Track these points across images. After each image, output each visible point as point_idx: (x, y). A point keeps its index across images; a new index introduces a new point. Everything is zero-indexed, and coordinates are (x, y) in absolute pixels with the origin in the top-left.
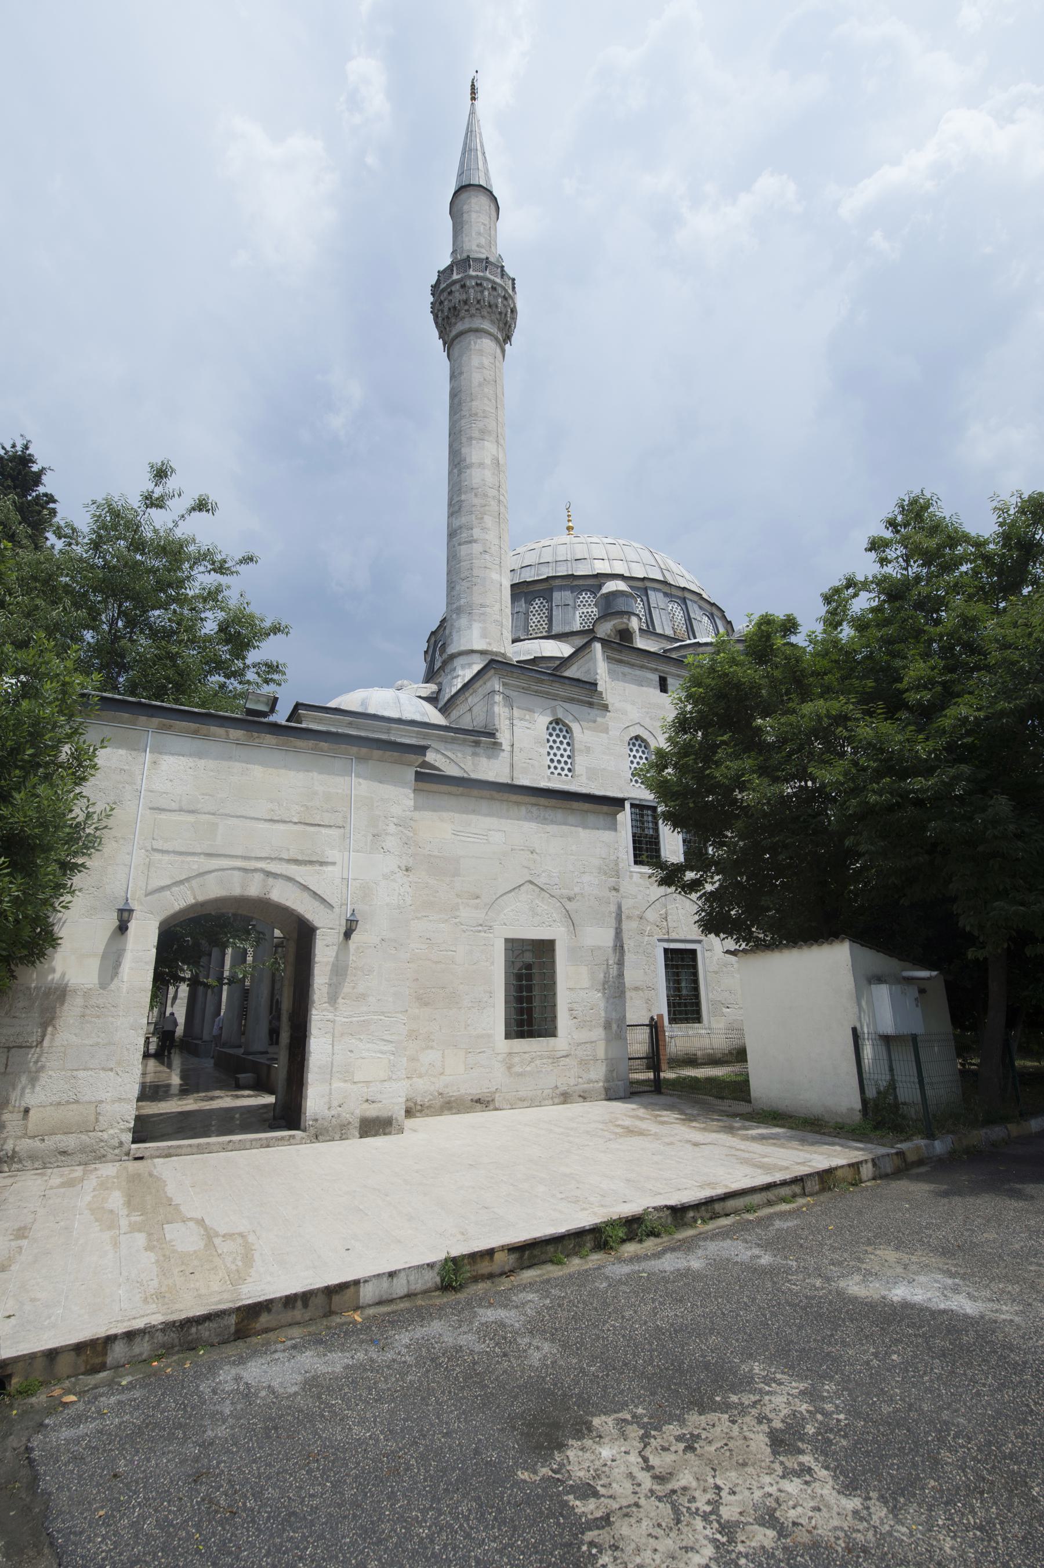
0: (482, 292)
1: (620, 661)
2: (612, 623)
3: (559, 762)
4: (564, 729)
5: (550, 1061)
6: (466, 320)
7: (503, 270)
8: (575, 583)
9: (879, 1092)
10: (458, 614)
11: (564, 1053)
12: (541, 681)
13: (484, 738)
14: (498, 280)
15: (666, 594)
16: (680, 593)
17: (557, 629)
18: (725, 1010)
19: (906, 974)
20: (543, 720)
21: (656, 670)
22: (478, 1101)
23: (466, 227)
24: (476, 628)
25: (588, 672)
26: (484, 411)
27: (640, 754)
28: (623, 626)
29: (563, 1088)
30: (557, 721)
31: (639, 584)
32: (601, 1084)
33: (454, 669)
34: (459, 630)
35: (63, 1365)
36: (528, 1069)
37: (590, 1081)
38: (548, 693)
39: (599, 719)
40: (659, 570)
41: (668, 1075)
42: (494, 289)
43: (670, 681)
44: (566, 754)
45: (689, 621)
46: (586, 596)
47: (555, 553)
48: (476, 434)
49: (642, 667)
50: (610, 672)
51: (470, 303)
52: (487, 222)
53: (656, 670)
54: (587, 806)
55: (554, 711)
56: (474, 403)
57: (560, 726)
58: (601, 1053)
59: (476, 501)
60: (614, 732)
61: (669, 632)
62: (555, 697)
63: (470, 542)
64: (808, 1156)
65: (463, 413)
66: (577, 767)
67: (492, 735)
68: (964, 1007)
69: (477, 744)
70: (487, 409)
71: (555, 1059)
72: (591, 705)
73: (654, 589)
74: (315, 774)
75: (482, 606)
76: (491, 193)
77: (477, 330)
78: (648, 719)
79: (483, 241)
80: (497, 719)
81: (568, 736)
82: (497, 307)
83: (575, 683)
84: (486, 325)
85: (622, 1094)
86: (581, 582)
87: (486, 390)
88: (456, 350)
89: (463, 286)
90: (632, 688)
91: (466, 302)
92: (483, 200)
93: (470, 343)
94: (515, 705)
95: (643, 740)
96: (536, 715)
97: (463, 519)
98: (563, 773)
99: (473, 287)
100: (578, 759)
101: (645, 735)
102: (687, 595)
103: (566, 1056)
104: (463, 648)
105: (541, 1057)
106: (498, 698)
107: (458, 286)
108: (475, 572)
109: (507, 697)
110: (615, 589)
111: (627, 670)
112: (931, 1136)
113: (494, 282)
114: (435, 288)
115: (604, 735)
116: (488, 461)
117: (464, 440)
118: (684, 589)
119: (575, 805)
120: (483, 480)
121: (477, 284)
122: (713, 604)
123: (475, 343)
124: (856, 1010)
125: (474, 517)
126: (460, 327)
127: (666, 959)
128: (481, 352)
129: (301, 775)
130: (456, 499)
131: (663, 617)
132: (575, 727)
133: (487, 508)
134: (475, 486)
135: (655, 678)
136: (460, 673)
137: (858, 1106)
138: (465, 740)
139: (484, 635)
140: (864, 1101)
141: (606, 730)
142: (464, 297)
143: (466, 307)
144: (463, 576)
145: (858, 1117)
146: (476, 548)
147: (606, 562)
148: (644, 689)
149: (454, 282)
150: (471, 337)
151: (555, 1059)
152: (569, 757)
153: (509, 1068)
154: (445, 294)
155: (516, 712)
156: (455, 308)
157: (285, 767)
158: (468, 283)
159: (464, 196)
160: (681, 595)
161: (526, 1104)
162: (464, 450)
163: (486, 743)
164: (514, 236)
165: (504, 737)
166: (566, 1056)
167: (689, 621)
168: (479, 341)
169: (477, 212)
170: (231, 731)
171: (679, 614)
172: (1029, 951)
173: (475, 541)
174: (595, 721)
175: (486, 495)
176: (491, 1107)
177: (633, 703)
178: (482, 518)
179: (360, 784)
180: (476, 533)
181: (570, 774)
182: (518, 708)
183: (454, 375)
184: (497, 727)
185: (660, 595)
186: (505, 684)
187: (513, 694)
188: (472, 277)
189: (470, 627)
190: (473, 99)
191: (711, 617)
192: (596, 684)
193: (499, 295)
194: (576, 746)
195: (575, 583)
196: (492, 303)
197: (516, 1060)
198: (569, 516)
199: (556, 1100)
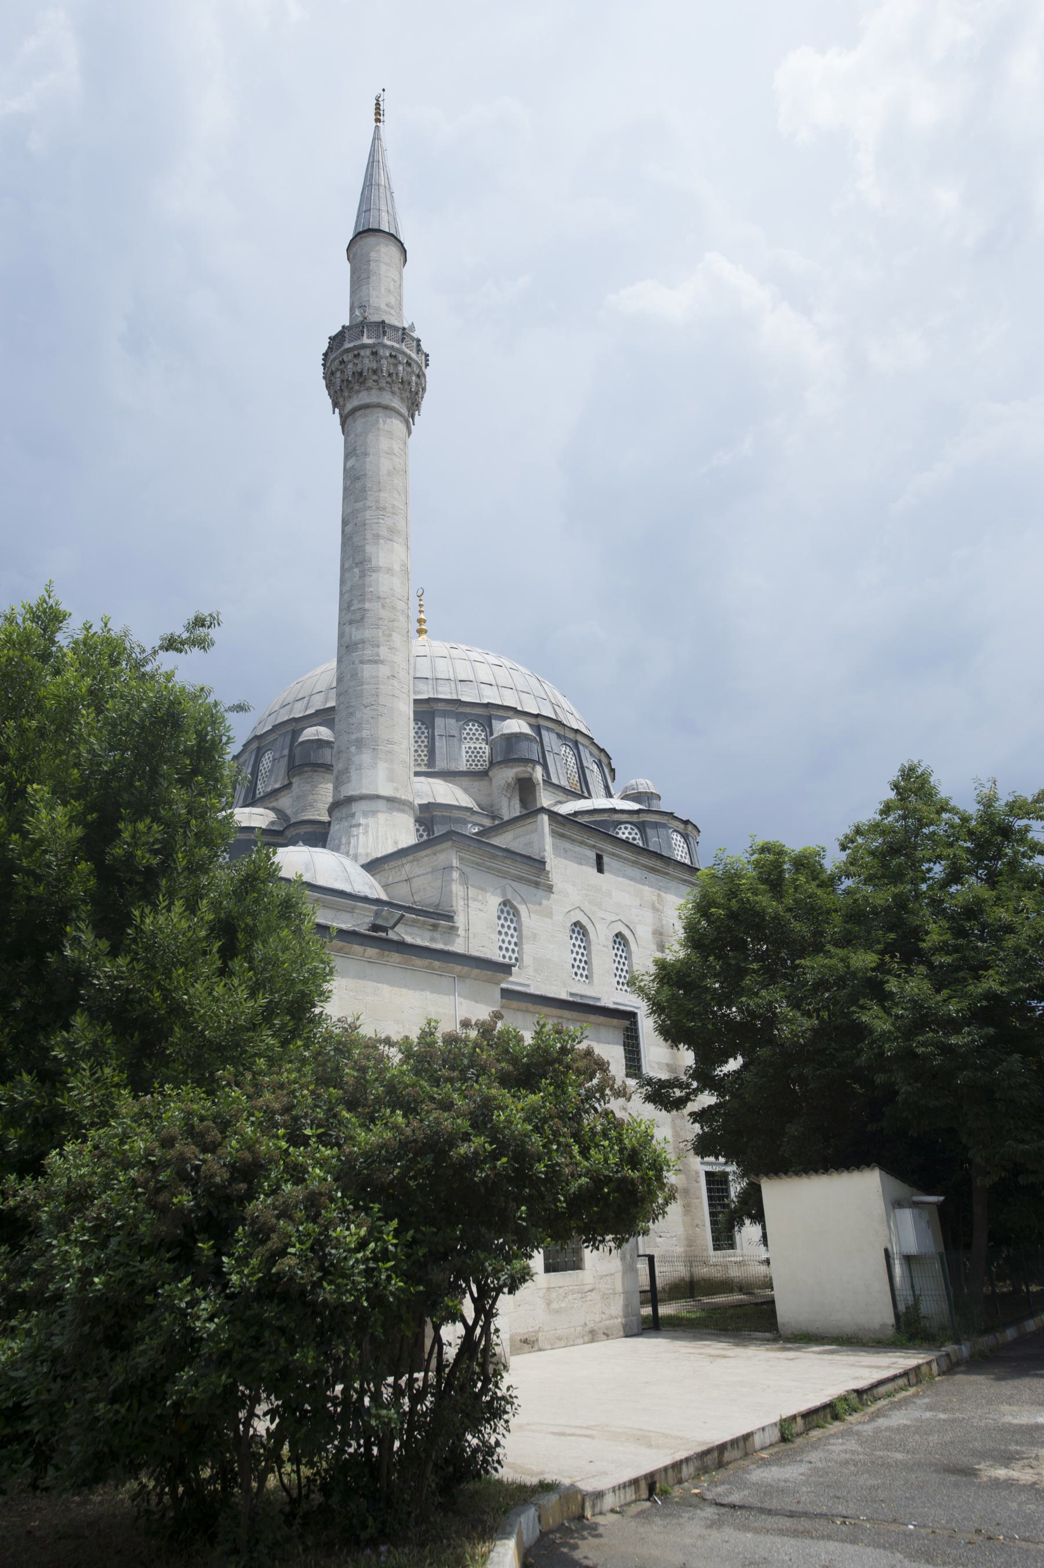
0: (396, 365)
1: (562, 836)
2: (515, 770)
3: (507, 949)
4: (511, 911)
5: (580, 1295)
6: (373, 392)
7: (419, 345)
8: (461, 710)
9: (907, 1308)
11: (590, 1287)
12: (494, 857)
13: (440, 917)
14: (414, 355)
15: (559, 735)
16: (571, 735)
17: (440, 765)
18: (659, 1240)
19: (916, 1198)
20: (494, 901)
21: (594, 846)
22: (525, 1341)
23: (373, 278)
24: (382, 768)
25: (530, 844)
26: (393, 506)
27: (579, 942)
28: (526, 775)
29: (590, 1325)
30: (505, 903)
31: (533, 721)
32: (619, 1320)
33: (353, 815)
34: (359, 768)
35: (687, 1471)
36: (563, 1305)
37: (611, 1317)
38: (499, 871)
39: (544, 902)
40: (550, 705)
41: (664, 1310)
42: (409, 364)
43: (606, 859)
45: (582, 769)
46: (473, 728)
47: (433, 668)
48: (384, 532)
49: (582, 843)
50: (555, 847)
51: (370, 371)
52: (396, 278)
53: (594, 846)
54: (602, 1019)
55: (504, 894)
56: (382, 494)
57: (508, 908)
58: (619, 1288)
59: (383, 613)
61: (564, 783)
63: (376, 662)
64: (894, 1360)
65: (368, 503)
67: (450, 918)
68: (953, 1227)
69: (435, 927)
70: (396, 503)
71: (584, 1293)
72: (537, 885)
73: (548, 729)
74: (428, 993)
75: (390, 742)
76: (402, 245)
77: (386, 408)
79: (393, 300)
80: (454, 899)
81: (515, 919)
82: (409, 383)
83: (525, 861)
84: (387, 399)
85: (636, 1331)
86: (468, 710)
87: (396, 481)
88: (359, 423)
89: (375, 353)
90: (573, 867)
91: (375, 372)
92: (393, 251)
93: (377, 421)
94: (470, 882)
95: (582, 927)
96: (488, 894)
97: (367, 631)
99: (386, 358)
100: (527, 947)
101: (585, 921)
102: (580, 739)
103: (591, 1291)
104: (365, 791)
105: (573, 1292)
106: (455, 875)
107: (368, 352)
108: (382, 700)
109: (463, 873)
110: (516, 730)
111: (567, 845)
112: (958, 1342)
113: (410, 358)
114: (336, 340)
116: (397, 568)
117: (369, 536)
118: (577, 731)
119: (593, 1018)
120: (392, 589)
121: (391, 355)
122: (602, 750)
123: (385, 423)
124: (887, 1232)
125: (380, 631)
126: (363, 398)
127: (708, 1183)
128: (390, 434)
129: (417, 994)
130: (356, 606)
131: (558, 764)
132: (522, 909)
133: (396, 624)
134: (382, 595)
135: (592, 855)
136: (362, 821)
137: (891, 1320)
138: (424, 923)
139: (391, 779)
140: (897, 1316)
141: (550, 915)
142: (374, 366)
143: (375, 377)
144: (365, 702)
145: (891, 1331)
146: (383, 670)
147: (448, 659)
148: (584, 867)
149: (365, 346)
150: (380, 414)
151: (584, 1293)
152: (516, 944)
153: (548, 1304)
154: (350, 356)
155: (472, 892)
156: (361, 374)
157: (406, 986)
158: (381, 352)
159: (371, 240)
160: (574, 739)
161: (563, 1343)
162: (369, 549)
163: (444, 927)
164: (419, 300)
165: (460, 920)
166: (591, 1291)
167: (582, 769)
168: (388, 420)
169: (386, 264)
170: (369, 949)
171: (572, 761)
172: (1022, 1180)
173: (382, 662)
174: (540, 904)
175: (394, 608)
176: (536, 1348)
178: (390, 636)
179: (461, 1004)
180: (383, 652)
182: (473, 886)
183: (350, 452)
184: (455, 908)
185: (553, 736)
186: (461, 859)
187: (467, 870)
188: (385, 346)
189: (374, 766)
190: (378, 120)
191: (600, 764)
192: (544, 863)
193: (413, 372)
194: (524, 932)
195: (461, 710)
196: (405, 379)
197: (554, 1295)
198: (420, 605)
199: (586, 1339)
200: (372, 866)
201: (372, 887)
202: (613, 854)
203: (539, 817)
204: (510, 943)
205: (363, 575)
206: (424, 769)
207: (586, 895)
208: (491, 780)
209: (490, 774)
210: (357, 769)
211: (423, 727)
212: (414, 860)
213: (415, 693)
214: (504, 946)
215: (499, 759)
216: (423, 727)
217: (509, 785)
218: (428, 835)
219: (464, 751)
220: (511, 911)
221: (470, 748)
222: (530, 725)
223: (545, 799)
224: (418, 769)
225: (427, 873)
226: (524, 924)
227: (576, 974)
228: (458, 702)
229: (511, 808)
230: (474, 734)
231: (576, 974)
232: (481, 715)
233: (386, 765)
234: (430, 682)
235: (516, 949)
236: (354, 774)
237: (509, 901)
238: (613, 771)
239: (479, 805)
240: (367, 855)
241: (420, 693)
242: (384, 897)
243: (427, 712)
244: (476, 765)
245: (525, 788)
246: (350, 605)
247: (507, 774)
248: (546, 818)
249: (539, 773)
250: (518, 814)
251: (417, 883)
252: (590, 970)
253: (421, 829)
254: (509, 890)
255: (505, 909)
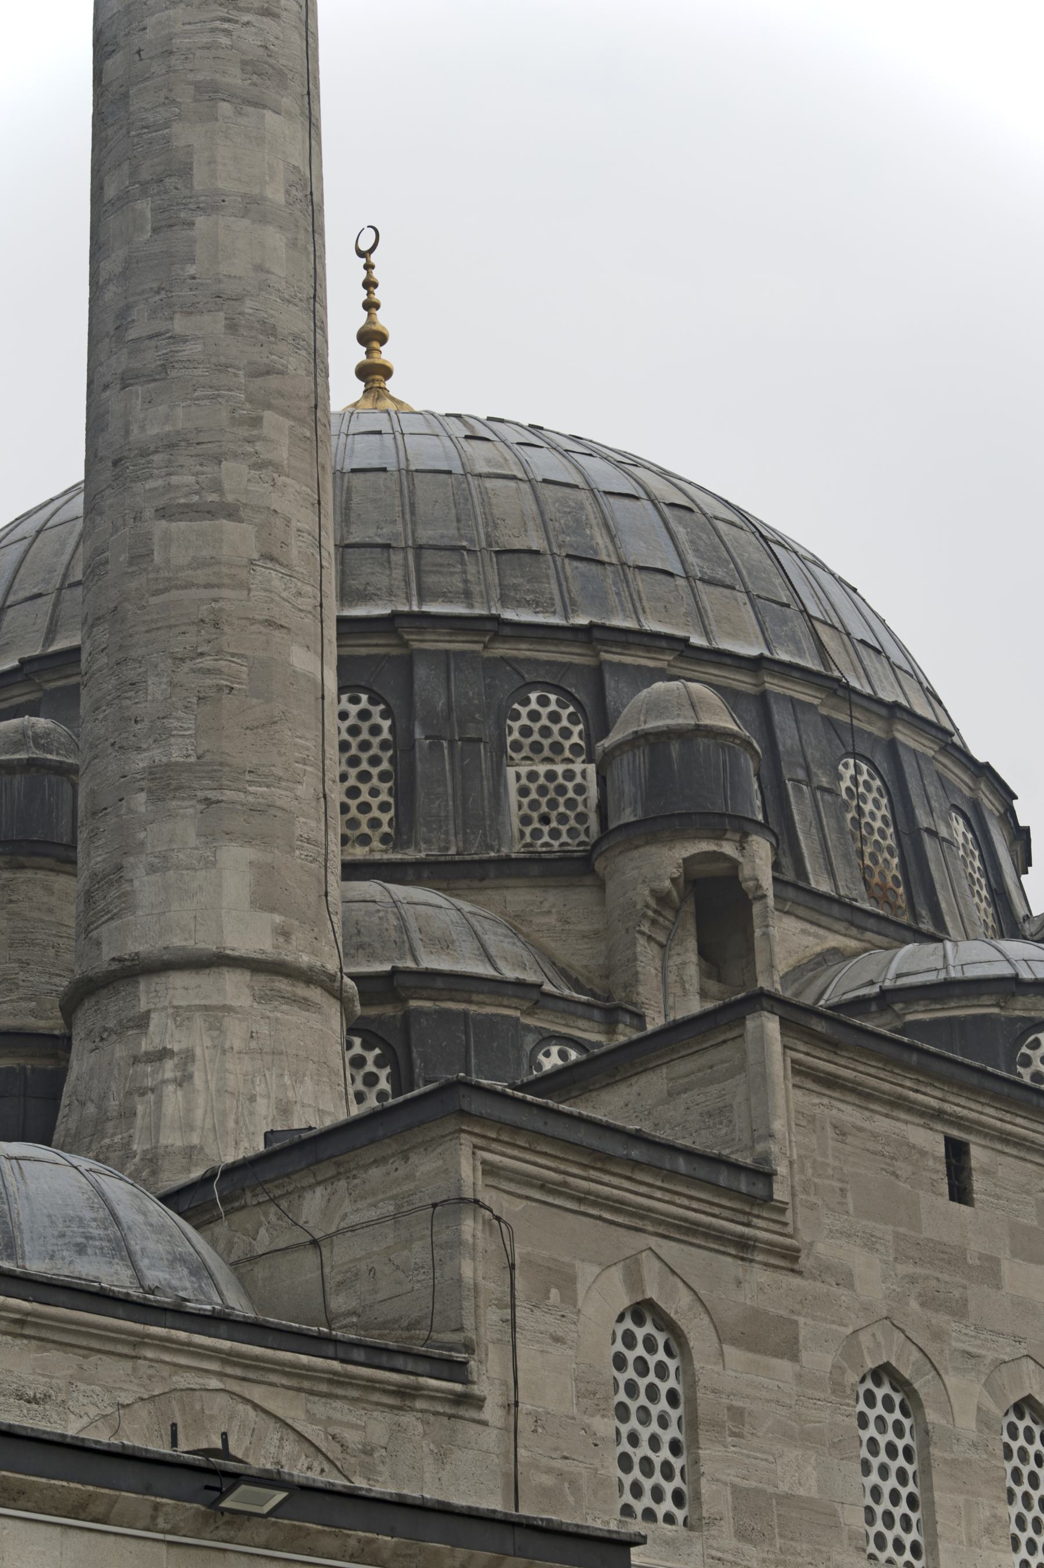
1: (830, 1082)
3: (647, 1465)
8: (501, 650)
10: (156, 797)
21: (939, 1115)
25: (721, 1113)
30: (642, 1310)
31: (742, 681)
33: (142, 1022)
38: (617, 1206)
43: (978, 1155)
44: (666, 1437)
45: (911, 838)
46: (538, 707)
49: (898, 1103)
53: (939, 1115)
55: (633, 1278)
57: (649, 1328)
60: (819, 1359)
62: (639, 1218)
63: (210, 512)
66: (706, 1488)
67: (455, 1369)
78: (914, 1305)
80: (468, 1304)
81: (672, 1364)
86: (523, 651)
95: (900, 1383)
98: (661, 1510)
102: (904, 736)
115: (784, 1366)
120: (259, 268)
133: (273, 382)
135: (932, 1142)
165: (488, 1377)
167: (911, 838)
177: (870, 1243)
178: (256, 422)
181: (680, 1514)
192: (768, 1176)
200: (191, 1201)
201: (200, 1270)
202: (1005, 1138)
203: (750, 1024)
204: (655, 1443)
205: (167, 222)
206: (377, 852)
207: (913, 1280)
208: (601, 886)
209: (599, 865)
210: (152, 869)
211: (377, 710)
212: (337, 1176)
213: (346, 596)
214: (637, 1455)
215: (628, 816)
216: (377, 710)
217: (662, 899)
218: (399, 1083)
219: (513, 787)
220: (661, 1338)
221: (543, 773)
222: (730, 695)
223: (787, 941)
224: (359, 853)
225: (380, 1221)
226: (703, 1381)
227: (880, 1541)
228: (496, 628)
229: (671, 986)
230: (545, 732)
231: (880, 1541)
232: (570, 666)
233: (250, 853)
234: (397, 558)
235: (677, 1463)
236: (144, 886)
237: (649, 1304)
238: (1021, 837)
239: (564, 974)
240: (190, 1153)
241: (364, 597)
242: (240, 1306)
243: (377, 657)
244: (555, 834)
245: (717, 909)
246: (123, 318)
247: (667, 861)
248: (772, 1025)
249: (759, 860)
250: (695, 1006)
251: (341, 1254)
252: (929, 1526)
253: (371, 1056)
254: (651, 1269)
255: (640, 1333)
